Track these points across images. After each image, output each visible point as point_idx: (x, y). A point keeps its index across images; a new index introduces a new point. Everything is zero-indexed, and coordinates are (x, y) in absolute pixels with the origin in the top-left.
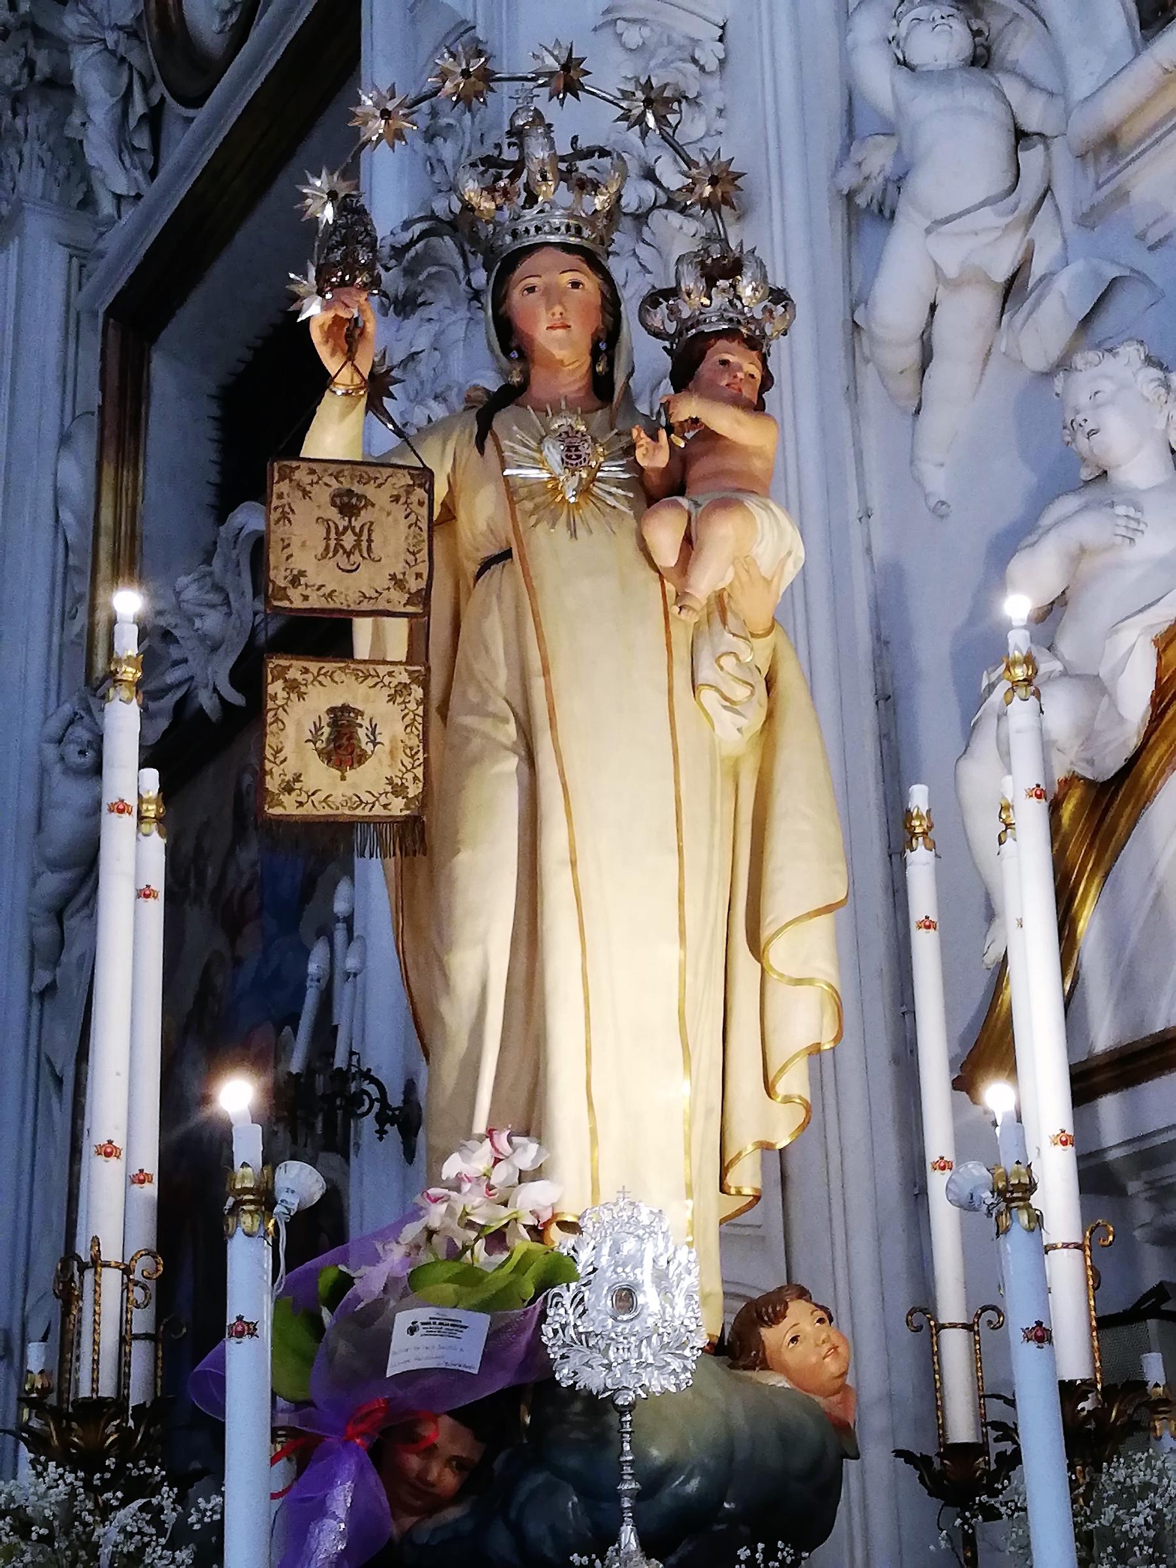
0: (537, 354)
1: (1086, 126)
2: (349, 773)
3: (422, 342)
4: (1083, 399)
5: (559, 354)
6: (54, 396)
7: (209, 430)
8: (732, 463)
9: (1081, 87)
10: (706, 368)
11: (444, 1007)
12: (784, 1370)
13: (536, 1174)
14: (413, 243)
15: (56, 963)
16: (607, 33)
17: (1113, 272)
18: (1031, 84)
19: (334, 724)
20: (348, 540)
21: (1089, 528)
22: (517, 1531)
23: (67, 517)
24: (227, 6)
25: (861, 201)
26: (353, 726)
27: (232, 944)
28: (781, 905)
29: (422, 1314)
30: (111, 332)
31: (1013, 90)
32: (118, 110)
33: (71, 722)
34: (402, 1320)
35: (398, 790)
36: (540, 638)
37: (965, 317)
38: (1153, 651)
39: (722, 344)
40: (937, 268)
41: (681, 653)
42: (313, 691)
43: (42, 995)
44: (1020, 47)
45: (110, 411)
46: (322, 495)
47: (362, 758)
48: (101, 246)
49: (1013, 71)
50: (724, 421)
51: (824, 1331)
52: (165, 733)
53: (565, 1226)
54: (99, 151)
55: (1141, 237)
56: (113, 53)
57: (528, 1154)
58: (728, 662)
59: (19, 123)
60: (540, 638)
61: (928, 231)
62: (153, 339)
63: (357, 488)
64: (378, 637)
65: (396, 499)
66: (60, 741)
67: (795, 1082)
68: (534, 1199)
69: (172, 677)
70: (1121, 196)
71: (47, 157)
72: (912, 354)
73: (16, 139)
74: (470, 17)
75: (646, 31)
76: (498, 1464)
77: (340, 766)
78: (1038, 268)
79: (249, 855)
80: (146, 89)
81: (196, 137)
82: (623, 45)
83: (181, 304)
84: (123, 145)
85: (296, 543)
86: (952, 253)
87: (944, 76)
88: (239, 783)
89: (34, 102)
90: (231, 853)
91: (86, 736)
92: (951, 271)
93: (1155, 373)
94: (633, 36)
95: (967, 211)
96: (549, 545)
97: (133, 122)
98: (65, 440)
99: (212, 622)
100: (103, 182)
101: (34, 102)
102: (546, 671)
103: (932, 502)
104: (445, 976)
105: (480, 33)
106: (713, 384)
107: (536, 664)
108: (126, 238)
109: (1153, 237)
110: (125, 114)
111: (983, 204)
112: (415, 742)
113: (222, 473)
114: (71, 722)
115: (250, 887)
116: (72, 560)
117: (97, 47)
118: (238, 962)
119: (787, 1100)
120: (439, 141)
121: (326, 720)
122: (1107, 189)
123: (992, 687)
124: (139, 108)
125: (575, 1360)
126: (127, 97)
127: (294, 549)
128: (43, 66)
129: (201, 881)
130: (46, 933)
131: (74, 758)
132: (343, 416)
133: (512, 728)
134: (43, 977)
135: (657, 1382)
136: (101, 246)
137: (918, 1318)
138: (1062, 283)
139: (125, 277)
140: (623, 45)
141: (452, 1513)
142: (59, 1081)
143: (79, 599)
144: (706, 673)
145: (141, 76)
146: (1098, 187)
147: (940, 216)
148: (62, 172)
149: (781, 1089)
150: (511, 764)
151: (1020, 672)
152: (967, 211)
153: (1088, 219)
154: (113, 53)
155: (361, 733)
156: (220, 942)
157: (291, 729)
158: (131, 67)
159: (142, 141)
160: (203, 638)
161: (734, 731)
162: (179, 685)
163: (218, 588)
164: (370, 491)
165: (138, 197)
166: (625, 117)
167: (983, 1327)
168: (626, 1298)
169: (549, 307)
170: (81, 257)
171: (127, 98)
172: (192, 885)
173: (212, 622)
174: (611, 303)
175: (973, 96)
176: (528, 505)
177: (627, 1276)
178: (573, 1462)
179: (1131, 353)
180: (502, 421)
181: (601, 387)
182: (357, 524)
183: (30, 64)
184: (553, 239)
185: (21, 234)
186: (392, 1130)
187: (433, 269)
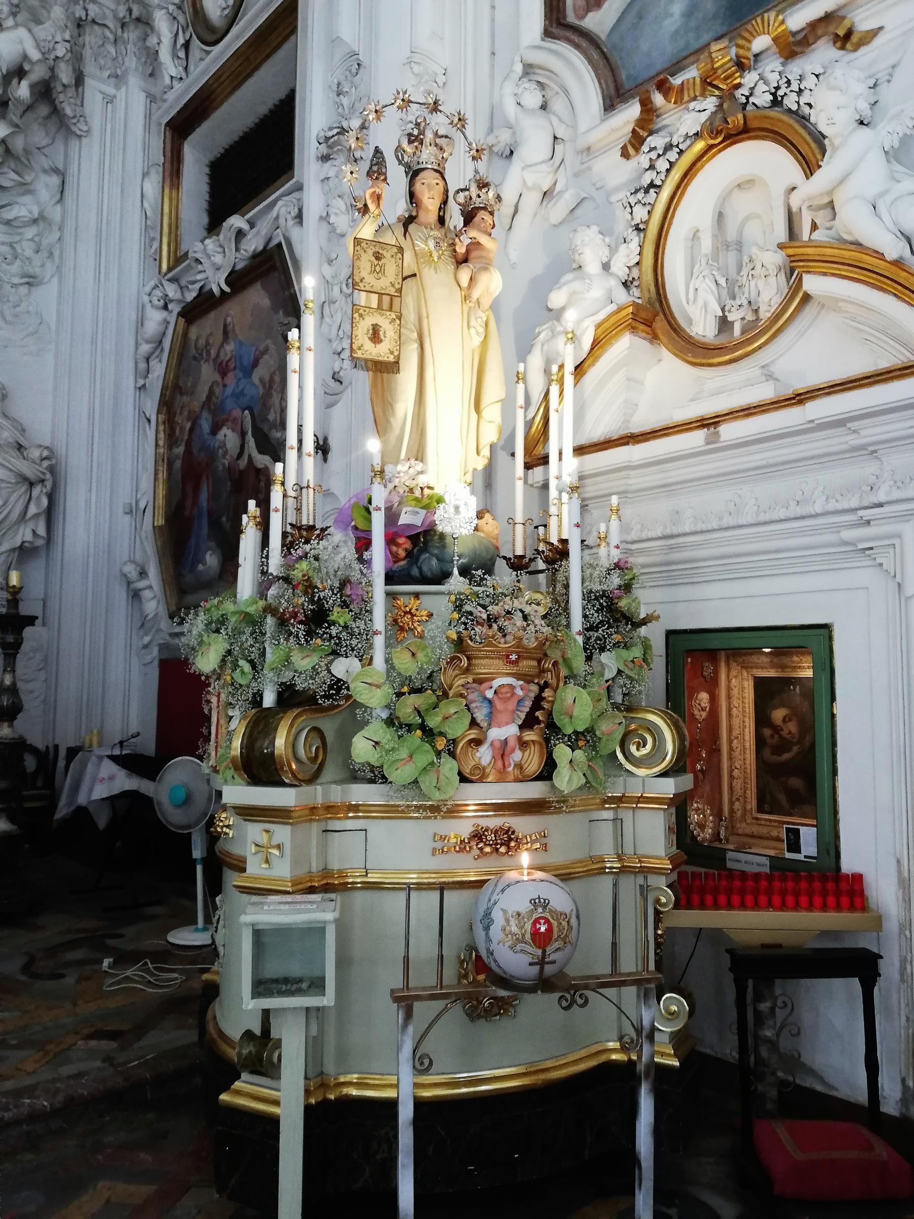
0: (423, 207)
1: (582, 143)
2: (377, 346)
3: (331, 174)
4: (579, 242)
5: (430, 207)
6: (140, 154)
7: (206, 179)
8: (484, 254)
9: (582, 128)
10: (477, 220)
11: (392, 420)
12: (483, 531)
13: (422, 472)
14: (333, 136)
15: (146, 377)
16: (407, 67)
17: (585, 195)
18: (560, 120)
19: (373, 329)
20: (378, 269)
21: (576, 286)
22: (420, 569)
23: (146, 205)
24: (224, 5)
25: (495, 149)
26: (378, 330)
27: (223, 378)
28: (486, 399)
29: (409, 509)
30: (167, 133)
31: (555, 120)
32: (173, 40)
33: (154, 288)
34: (404, 510)
35: (392, 353)
36: (426, 307)
37: (531, 200)
38: (594, 329)
39: (482, 212)
40: (524, 182)
41: (465, 315)
42: (367, 318)
43: (140, 388)
44: (558, 105)
45: (168, 166)
46: (370, 252)
47: (381, 341)
48: (165, 97)
49: (554, 114)
50: (483, 239)
51: (494, 522)
52: (195, 298)
53: (429, 488)
54: (165, 55)
55: (594, 185)
56: (171, 14)
57: (419, 466)
58: (479, 320)
59: (125, 35)
60: (426, 307)
61: (523, 169)
62: (185, 139)
63: (381, 252)
64: (368, 299)
65: (392, 256)
66: (149, 295)
67: (486, 452)
68: (422, 480)
69: (199, 277)
70: (589, 169)
71: (137, 52)
72: (512, 210)
73: (124, 42)
74: (356, 50)
75: (421, 68)
76: (415, 551)
77: (375, 343)
78: (558, 187)
79: (230, 348)
80: (184, 32)
81: (209, 62)
82: (413, 72)
83: (199, 126)
84: (175, 56)
85: (362, 267)
86: (531, 178)
87: (531, 112)
88: (225, 320)
89: (132, 27)
90: (222, 345)
91: (160, 294)
92: (530, 184)
93: (601, 236)
94: (416, 69)
95: (536, 164)
96: (428, 275)
97: (179, 46)
98: (145, 175)
99: (218, 259)
100: (166, 70)
101: (132, 27)
102: (428, 318)
103: (512, 262)
104: (393, 411)
105: (361, 57)
106: (479, 225)
107: (425, 315)
108: (178, 96)
109: (598, 185)
110: (175, 42)
111: (541, 163)
112: (397, 338)
113: (210, 197)
114: (154, 288)
115: (230, 360)
116: (148, 222)
117: (164, 11)
118: (225, 386)
119: (483, 456)
120: (342, 96)
121: (371, 328)
122: (585, 165)
123: (539, 333)
124: (181, 41)
125: (443, 524)
126: (177, 34)
127: (361, 270)
128: (136, 13)
129: (208, 353)
130: (142, 366)
131: (156, 302)
132: (371, 224)
133: (415, 334)
134: (141, 382)
135: (464, 532)
136: (165, 97)
137: (510, 521)
138: (567, 196)
139: (176, 111)
140: (413, 72)
141: (402, 563)
142: (149, 421)
143: (153, 239)
144: (473, 323)
145: (183, 27)
146: (582, 163)
147: (529, 163)
148: (143, 59)
149: (482, 453)
150: (415, 346)
151: (570, 336)
152: (536, 164)
153: (577, 175)
154: (171, 14)
155: (381, 333)
156: (218, 377)
157: (360, 329)
158: (178, 22)
159: (182, 54)
160: (214, 264)
161: (477, 340)
162: (201, 280)
163: (221, 246)
164: (384, 253)
165: (181, 79)
166: (452, 123)
167: (527, 524)
168: (457, 508)
169: (429, 191)
170: (152, 98)
171: (177, 34)
172: (204, 355)
173: (218, 259)
174: (446, 191)
175: (541, 120)
176: (422, 260)
177: (457, 503)
178: (436, 552)
179: (595, 229)
180: (412, 227)
181: (441, 221)
182: (380, 263)
183: (130, 11)
184: (430, 166)
185: (126, 84)
186: (320, 452)
187: (340, 147)
